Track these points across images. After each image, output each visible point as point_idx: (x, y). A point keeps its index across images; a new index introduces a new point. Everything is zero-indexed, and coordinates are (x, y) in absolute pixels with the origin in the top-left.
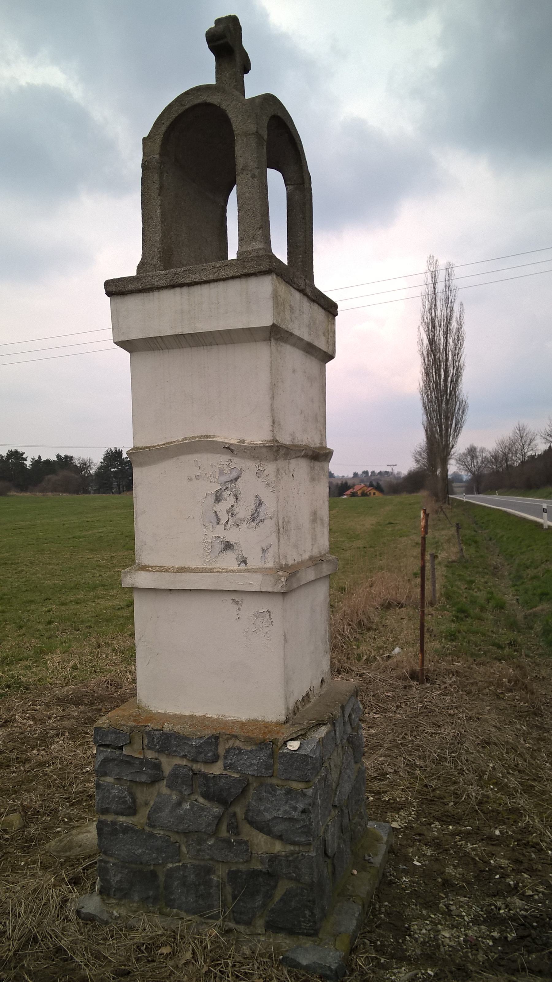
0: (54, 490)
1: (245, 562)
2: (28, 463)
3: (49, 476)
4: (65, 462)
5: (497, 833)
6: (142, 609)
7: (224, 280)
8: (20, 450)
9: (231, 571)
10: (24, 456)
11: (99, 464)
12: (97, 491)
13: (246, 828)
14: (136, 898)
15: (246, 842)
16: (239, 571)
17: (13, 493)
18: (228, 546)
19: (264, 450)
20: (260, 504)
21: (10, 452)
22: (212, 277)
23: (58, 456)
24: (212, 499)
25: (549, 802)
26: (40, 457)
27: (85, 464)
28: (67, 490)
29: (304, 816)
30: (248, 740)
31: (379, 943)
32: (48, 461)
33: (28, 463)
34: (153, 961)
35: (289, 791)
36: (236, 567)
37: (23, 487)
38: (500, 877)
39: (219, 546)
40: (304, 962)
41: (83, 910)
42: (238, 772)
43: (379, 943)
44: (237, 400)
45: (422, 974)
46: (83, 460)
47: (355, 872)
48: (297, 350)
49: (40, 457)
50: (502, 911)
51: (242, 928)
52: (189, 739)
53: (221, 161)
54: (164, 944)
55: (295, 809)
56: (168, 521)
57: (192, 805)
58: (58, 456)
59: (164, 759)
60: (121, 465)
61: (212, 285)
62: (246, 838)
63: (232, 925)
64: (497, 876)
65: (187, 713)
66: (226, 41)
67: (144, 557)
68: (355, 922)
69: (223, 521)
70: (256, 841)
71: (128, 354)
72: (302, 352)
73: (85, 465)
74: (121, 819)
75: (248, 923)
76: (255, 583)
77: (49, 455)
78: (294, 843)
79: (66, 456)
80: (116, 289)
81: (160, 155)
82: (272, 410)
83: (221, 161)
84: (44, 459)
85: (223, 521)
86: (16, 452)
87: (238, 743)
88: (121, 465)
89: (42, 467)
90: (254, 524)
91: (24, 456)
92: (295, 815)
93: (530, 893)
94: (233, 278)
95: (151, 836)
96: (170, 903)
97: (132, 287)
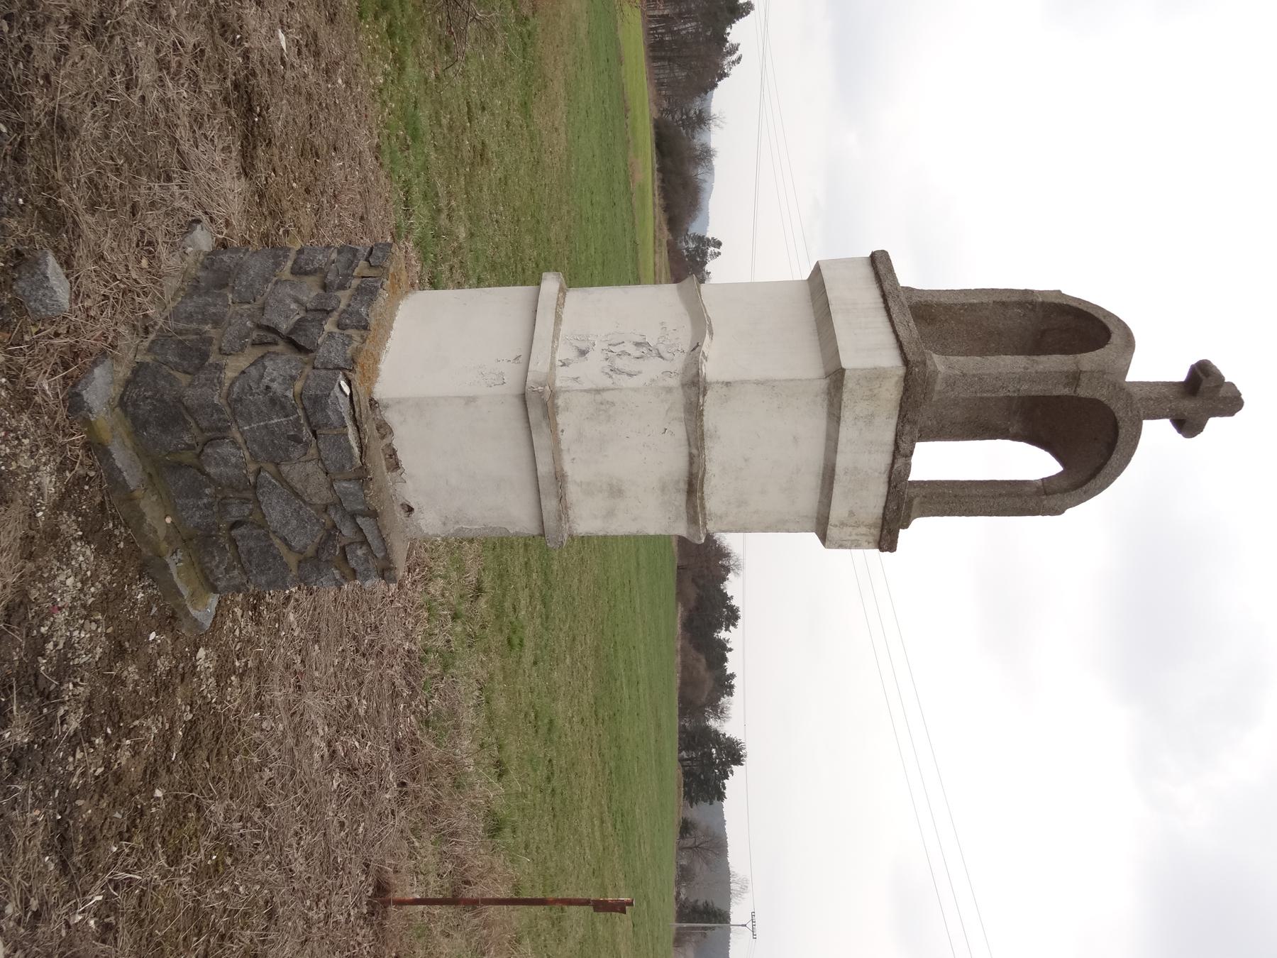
0: (686, 667)
1: (564, 365)
2: (723, 634)
3: (704, 660)
4: (724, 685)
5: (158, 793)
6: (518, 293)
7: (895, 332)
8: (740, 622)
9: (553, 352)
10: (731, 628)
11: (722, 731)
12: (683, 730)
13: (258, 352)
14: (200, 274)
15: (242, 350)
16: (553, 358)
17: (680, 609)
18: (583, 353)
19: (694, 371)
20: (630, 375)
21: (737, 610)
22: (896, 321)
23: (732, 676)
24: (639, 339)
25: (315, 17)
26: (731, 650)
27: (722, 712)
28: (685, 684)
29: (262, 388)
30: (358, 350)
31: (87, 488)
32: (725, 660)
33: (723, 634)
34: (138, 245)
35: (293, 378)
36: (557, 358)
37: (688, 625)
38: (107, 734)
39: (583, 346)
40: (97, 371)
41: (199, 227)
42: (323, 342)
43: (87, 488)
44: (761, 443)
45: (42, 505)
46: (728, 709)
47: (168, 520)
48: (822, 457)
49: (731, 650)
50: (71, 686)
51: (146, 344)
52: (369, 305)
53: (1050, 389)
54: (150, 265)
55: (273, 380)
56: (616, 321)
57: (293, 311)
58: (732, 676)
59: (348, 292)
60: (722, 763)
61: (888, 324)
62: (246, 351)
63: (152, 337)
64: (109, 731)
65: (395, 325)
66: (1202, 397)
67: (574, 296)
68: (120, 465)
69: (612, 348)
70: (241, 359)
71: (806, 277)
72: (822, 463)
73: (719, 712)
74: (290, 263)
75: (149, 350)
76: (539, 366)
77: (732, 664)
78: (232, 385)
79: (732, 687)
80: (879, 264)
81: (1043, 303)
82: (743, 382)
83: (1050, 389)
84: (728, 655)
85: (612, 348)
86: (737, 618)
87: (355, 344)
88: (722, 763)
89: (718, 653)
90: (607, 370)
91: (731, 628)
92: (266, 381)
93: (79, 755)
94: (897, 336)
95: (267, 281)
96: (189, 296)
97: (887, 286)
